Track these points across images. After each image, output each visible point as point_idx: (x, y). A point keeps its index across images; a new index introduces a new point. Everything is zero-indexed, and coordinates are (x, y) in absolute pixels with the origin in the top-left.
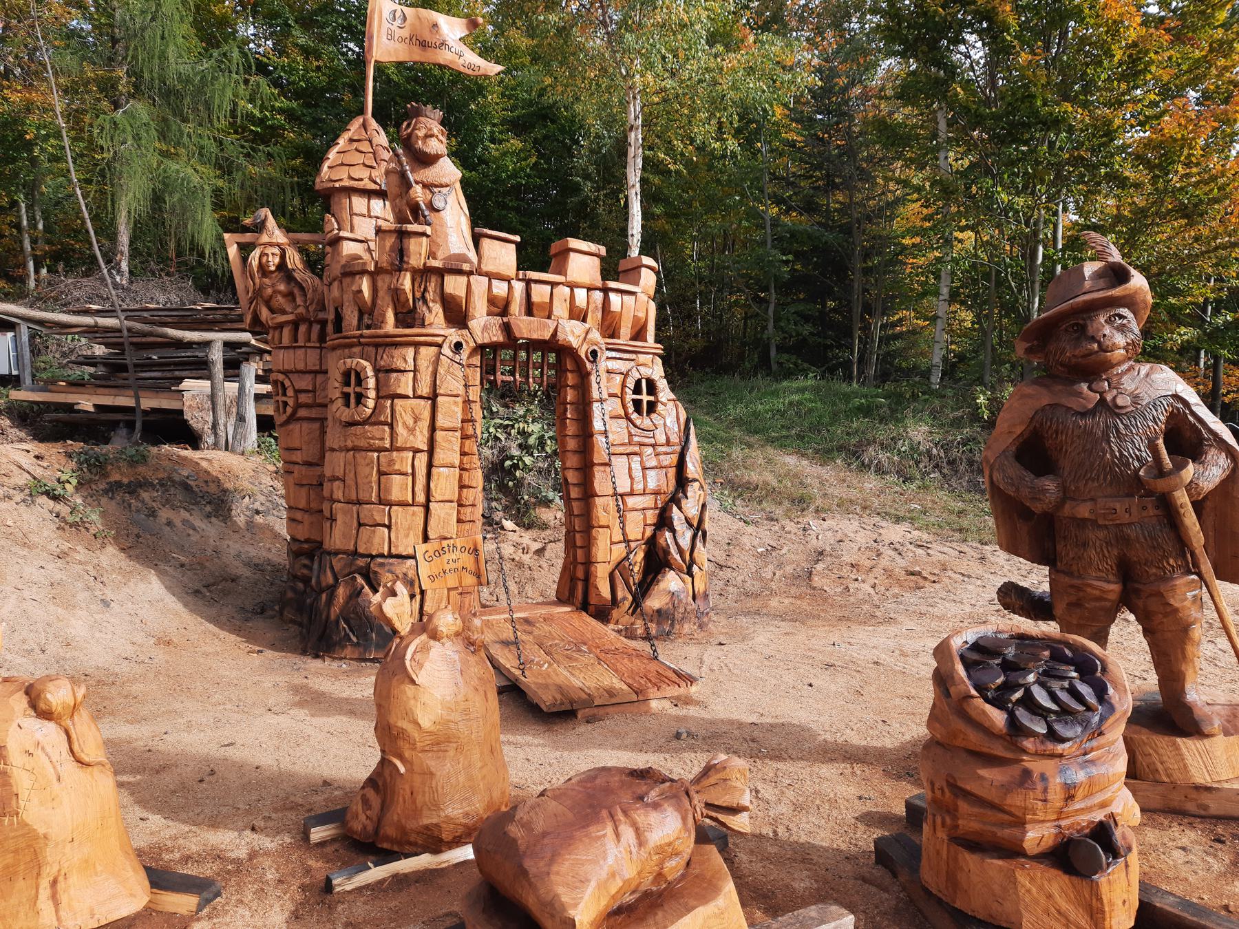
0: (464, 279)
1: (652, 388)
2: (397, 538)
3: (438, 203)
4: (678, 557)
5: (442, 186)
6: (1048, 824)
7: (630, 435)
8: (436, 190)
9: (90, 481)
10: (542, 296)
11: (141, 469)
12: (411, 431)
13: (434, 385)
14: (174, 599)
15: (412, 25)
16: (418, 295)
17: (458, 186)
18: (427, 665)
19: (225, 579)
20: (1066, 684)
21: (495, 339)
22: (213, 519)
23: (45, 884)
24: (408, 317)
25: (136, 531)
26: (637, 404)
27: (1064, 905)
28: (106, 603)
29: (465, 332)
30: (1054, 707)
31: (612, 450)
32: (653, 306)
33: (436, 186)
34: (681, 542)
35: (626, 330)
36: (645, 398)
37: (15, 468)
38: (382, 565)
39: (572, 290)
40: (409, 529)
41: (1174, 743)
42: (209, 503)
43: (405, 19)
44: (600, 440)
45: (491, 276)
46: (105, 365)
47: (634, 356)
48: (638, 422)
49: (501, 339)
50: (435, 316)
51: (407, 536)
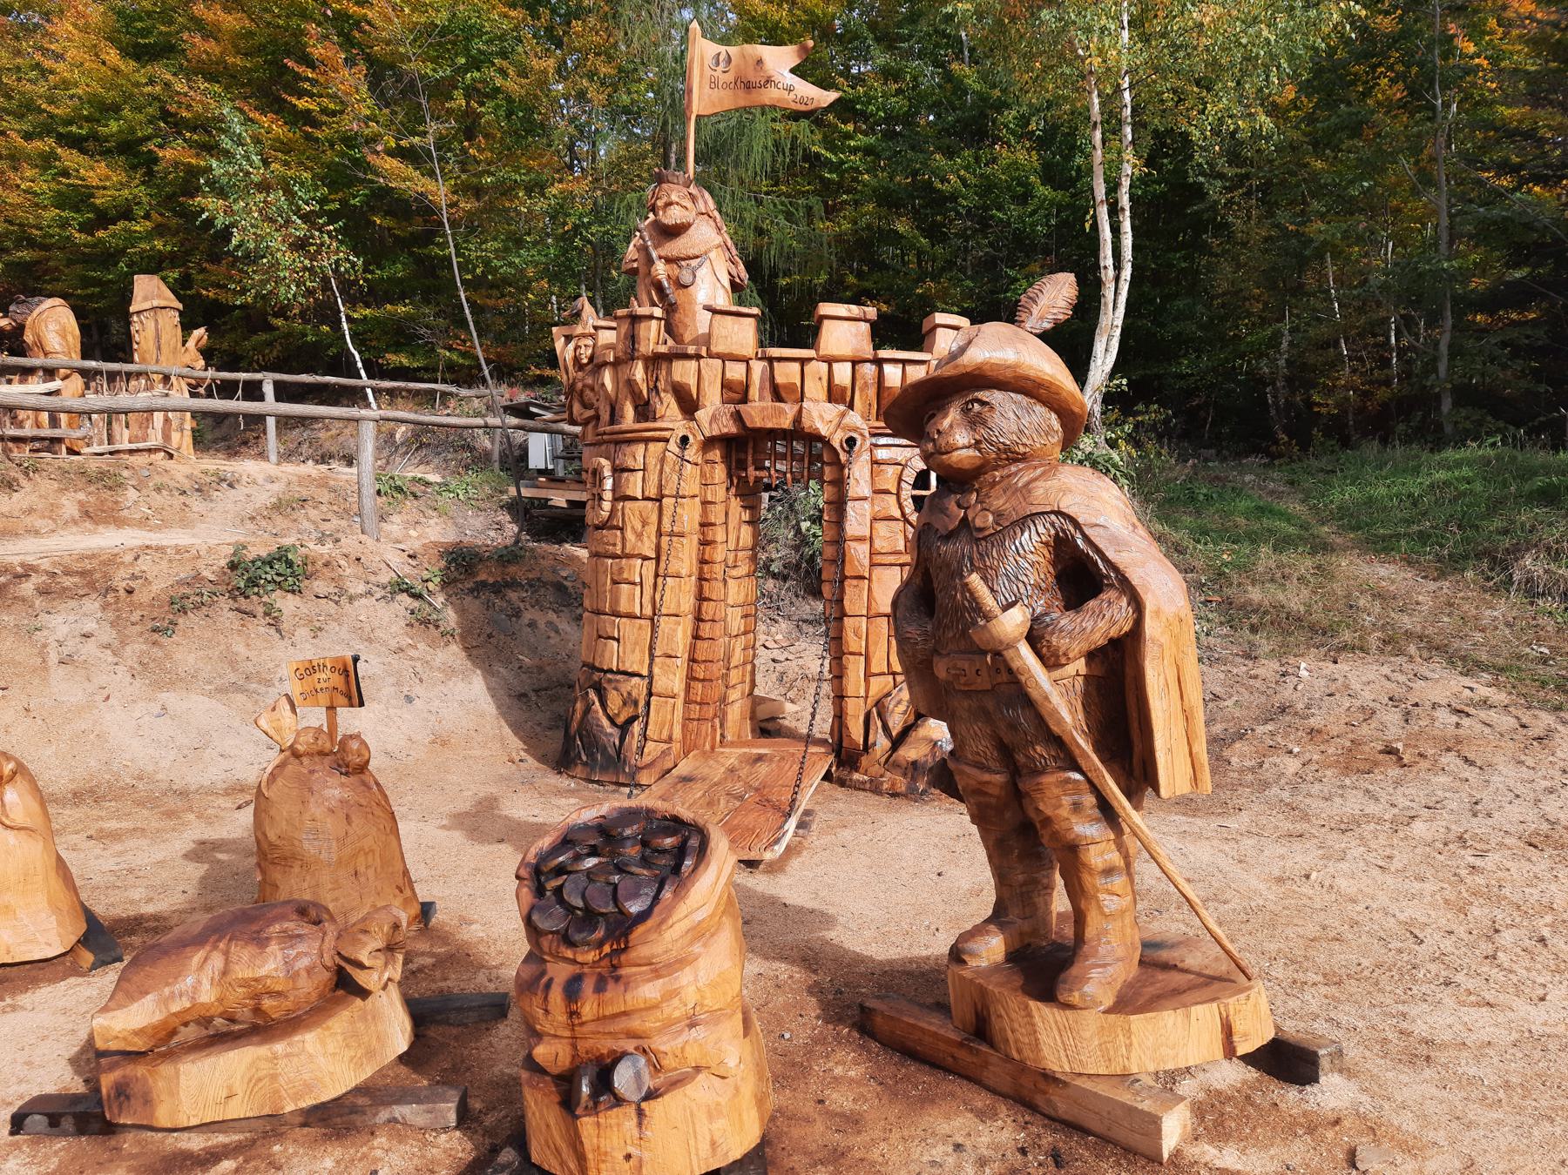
0: (693, 364)
3: (686, 278)
5: (690, 258)
9: (455, 581)
10: (787, 375)
11: (512, 569)
12: (639, 536)
13: (660, 486)
14: (490, 700)
15: (738, 66)
16: (651, 385)
19: (562, 685)
21: (725, 430)
24: (645, 411)
27: (559, 1141)
28: (409, 699)
31: (878, 559)
37: (383, 566)
38: (610, 681)
40: (636, 643)
41: (1027, 1007)
43: (729, 60)
45: (725, 358)
49: (734, 430)
50: (668, 407)
51: (633, 651)
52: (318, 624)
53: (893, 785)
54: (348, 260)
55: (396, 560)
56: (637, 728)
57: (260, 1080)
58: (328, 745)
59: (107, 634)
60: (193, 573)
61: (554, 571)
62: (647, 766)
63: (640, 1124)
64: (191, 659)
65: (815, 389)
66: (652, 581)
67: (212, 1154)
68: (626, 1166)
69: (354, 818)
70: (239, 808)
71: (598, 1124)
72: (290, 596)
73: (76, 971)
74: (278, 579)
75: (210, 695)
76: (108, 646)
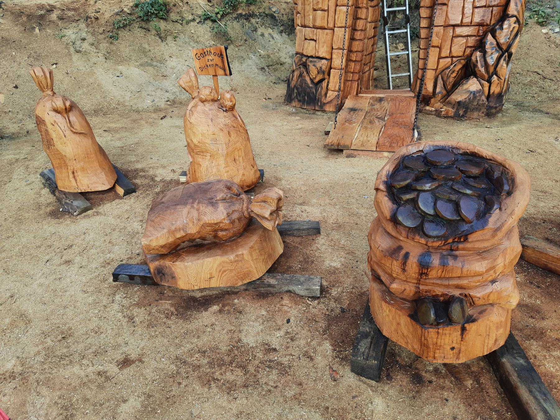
2: (319, 47)
4: (483, 70)
6: (411, 284)
11: (252, 7)
19: (278, 64)
22: (283, 34)
23: (70, 172)
25: (245, 38)
38: (311, 62)
42: (282, 25)
51: (323, 46)
52: (175, 35)
53: (447, 112)
56: (324, 84)
57: (225, 271)
58: (216, 96)
59: (90, 39)
60: (120, 10)
61: (270, 9)
62: (328, 103)
63: (462, 334)
64: (127, 50)
66: (334, 8)
68: (451, 352)
70: (162, 119)
71: (438, 333)
72: (162, 21)
73: (118, 197)
74: (156, 12)
75: (138, 67)
76: (93, 44)
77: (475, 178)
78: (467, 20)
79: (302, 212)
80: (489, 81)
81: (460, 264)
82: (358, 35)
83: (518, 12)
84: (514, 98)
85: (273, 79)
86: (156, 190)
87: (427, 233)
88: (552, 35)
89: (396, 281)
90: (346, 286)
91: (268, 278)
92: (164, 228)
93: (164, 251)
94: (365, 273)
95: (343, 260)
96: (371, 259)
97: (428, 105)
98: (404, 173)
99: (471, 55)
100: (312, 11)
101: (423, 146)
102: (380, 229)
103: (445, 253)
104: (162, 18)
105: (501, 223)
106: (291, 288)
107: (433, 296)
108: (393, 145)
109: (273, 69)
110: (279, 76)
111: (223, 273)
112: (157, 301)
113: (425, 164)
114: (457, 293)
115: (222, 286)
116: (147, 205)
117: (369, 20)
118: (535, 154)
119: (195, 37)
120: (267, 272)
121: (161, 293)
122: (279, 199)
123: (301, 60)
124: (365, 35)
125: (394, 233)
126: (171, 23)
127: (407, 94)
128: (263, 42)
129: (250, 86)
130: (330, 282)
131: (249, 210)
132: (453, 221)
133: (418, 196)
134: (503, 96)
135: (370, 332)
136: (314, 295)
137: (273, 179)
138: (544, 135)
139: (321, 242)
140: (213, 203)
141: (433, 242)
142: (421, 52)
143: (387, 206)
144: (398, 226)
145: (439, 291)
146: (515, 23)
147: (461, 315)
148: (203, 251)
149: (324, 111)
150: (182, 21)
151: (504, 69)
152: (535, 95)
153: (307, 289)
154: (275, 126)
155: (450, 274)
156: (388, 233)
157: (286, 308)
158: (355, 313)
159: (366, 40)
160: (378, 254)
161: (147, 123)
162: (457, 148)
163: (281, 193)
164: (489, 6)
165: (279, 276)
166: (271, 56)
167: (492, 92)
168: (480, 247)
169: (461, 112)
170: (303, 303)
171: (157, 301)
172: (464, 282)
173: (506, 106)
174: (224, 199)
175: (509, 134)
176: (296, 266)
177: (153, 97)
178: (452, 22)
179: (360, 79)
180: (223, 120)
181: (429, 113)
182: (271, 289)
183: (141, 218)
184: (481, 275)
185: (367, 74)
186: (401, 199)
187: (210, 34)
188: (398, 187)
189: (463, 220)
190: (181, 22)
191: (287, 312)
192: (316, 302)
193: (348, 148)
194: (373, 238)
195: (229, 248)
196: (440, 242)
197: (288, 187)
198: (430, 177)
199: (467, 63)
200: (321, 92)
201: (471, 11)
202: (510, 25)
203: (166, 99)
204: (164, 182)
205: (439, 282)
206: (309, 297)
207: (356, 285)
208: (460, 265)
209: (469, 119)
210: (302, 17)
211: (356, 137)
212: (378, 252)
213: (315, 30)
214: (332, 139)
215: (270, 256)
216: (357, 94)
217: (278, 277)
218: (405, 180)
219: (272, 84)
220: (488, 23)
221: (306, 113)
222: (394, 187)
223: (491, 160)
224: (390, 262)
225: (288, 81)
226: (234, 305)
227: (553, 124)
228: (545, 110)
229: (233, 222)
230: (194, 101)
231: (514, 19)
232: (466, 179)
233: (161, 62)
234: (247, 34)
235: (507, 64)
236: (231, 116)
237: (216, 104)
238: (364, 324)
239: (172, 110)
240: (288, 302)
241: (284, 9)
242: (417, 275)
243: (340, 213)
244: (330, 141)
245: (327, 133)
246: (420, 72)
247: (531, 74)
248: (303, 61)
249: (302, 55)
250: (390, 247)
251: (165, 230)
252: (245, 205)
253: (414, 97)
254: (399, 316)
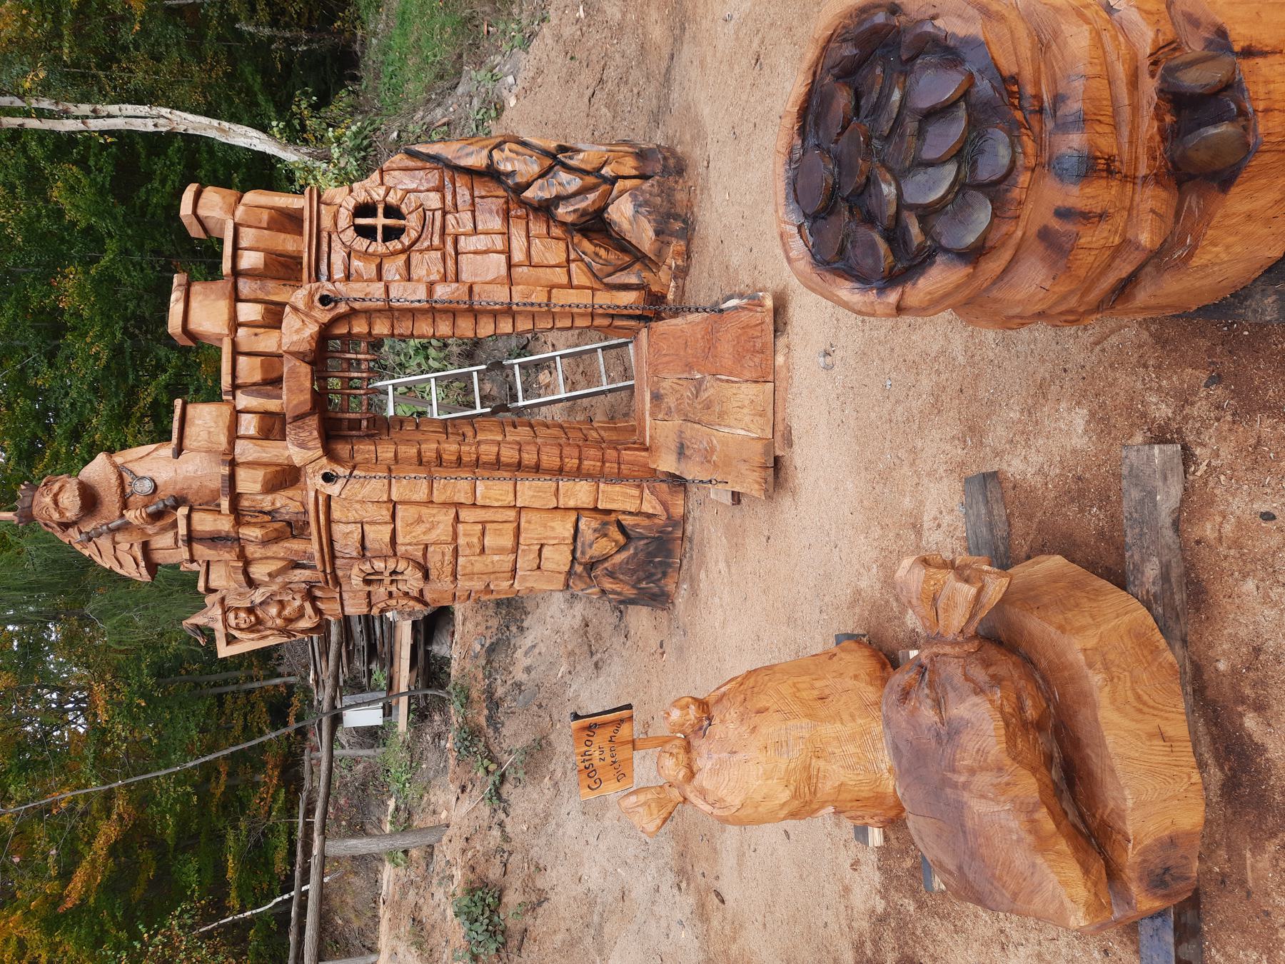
1: (365, 209)
2: (555, 538)
4: (592, 197)
6: (1137, 198)
7: (431, 248)
8: (128, 490)
10: (252, 369)
11: (474, 694)
17: (119, 458)
18: (722, 793)
20: (911, 126)
21: (315, 433)
22: (525, 624)
24: (295, 529)
26: (392, 234)
29: (309, 470)
30: (950, 171)
31: (451, 274)
32: (251, 197)
33: (123, 490)
34: (572, 188)
35: (288, 243)
36: (380, 221)
38: (583, 553)
39: (241, 325)
44: (441, 291)
45: (233, 434)
46: (369, 663)
47: (325, 234)
48: (414, 234)
51: (553, 529)
52: (533, 868)
53: (679, 254)
54: (179, 917)
55: (466, 805)
56: (628, 521)
57: (1139, 698)
58: (677, 742)
62: (667, 510)
63: (1264, 54)
65: (268, 342)
66: (479, 511)
67: (1229, 750)
69: (760, 705)
70: (723, 902)
71: (1267, 111)
72: (505, 900)
77: (858, 96)
78: (499, 242)
79: (939, 526)
80: (613, 181)
81: (1076, 84)
82: (529, 457)
83: (483, 148)
84: (641, 133)
85: (617, 641)
86: (912, 909)
87: (1004, 171)
88: (520, 87)
89: (1129, 235)
90: (1139, 385)
91: (1142, 584)
92: (1034, 865)
93: (1098, 866)
94: (1096, 344)
95: (1063, 405)
96: (1070, 312)
97: (664, 297)
98: (856, 255)
99: (563, 224)
100: (484, 557)
101: (788, 228)
102: (995, 293)
103: (1050, 125)
104: (500, 900)
105: (969, 7)
106: (1165, 519)
107: (1164, 139)
108: (759, 345)
109: (597, 641)
110: (610, 628)
111: (1145, 704)
112: (1249, 894)
113: (830, 214)
114: (1150, 86)
115: (1182, 706)
116: (957, 932)
117: (499, 438)
118: (763, 51)
119: (537, 821)
120: (1124, 588)
121: (1223, 882)
122: (925, 562)
123: (580, 576)
124: (529, 444)
125: (1006, 255)
126: (509, 877)
127: (640, 351)
128: (543, 668)
129: (636, 691)
130: (1132, 425)
131: (960, 639)
132: (969, 115)
133: (912, 207)
134: (642, 150)
135: (1276, 292)
136: (1178, 460)
137: (857, 610)
138: (720, 48)
139: (1017, 466)
140: (950, 733)
141: (1024, 153)
142: (559, 325)
143: (939, 278)
144: (989, 244)
145: (1148, 127)
146: (503, 151)
147: (1210, 64)
148: (1085, 759)
149: (684, 518)
150: (503, 852)
151: (588, 155)
152: (635, 91)
153: (1165, 479)
154: (724, 624)
155: (1105, 103)
156: (1005, 271)
157: (1228, 528)
158: (1218, 349)
159: (539, 441)
160: (1062, 289)
161: (734, 940)
162: (791, 152)
163: (907, 562)
164: (473, 204)
165: (1133, 556)
166: (570, 648)
167: (634, 172)
168: (1029, 45)
169: (677, 225)
170: (1206, 484)
171: (1249, 894)
172: (1121, 71)
173: (659, 139)
174: (938, 705)
175: (720, 116)
176: (1095, 517)
177: (673, 924)
178: (503, 271)
179: (615, 446)
180: (732, 726)
181: (681, 291)
182: (1175, 573)
183: (996, 949)
184: (1097, 36)
185: (605, 439)
186: (921, 248)
187: (530, 788)
188: (891, 259)
189: (965, 95)
190: (506, 855)
191: (1239, 524)
192: (1198, 451)
193: (769, 445)
194: (1017, 310)
195: (1070, 689)
196: (1025, 138)
197: (874, 570)
198: (862, 193)
199: (579, 231)
200: (644, 527)
201: (482, 237)
202: (507, 159)
203: (675, 891)
204: (887, 890)
205: (1125, 131)
206: (1185, 472)
207: (1134, 360)
208: (1079, 85)
209: (690, 206)
210: (497, 579)
211: (743, 432)
212: (1056, 289)
213: (521, 547)
214: (750, 484)
215: (1076, 585)
216: (647, 450)
217: (1136, 557)
218: (873, 246)
219: (629, 643)
220: (503, 200)
221: (691, 557)
222: (891, 269)
223: (815, 73)
224: (1082, 254)
225: (623, 604)
226: (1234, 671)
227: (694, 38)
228: (664, 65)
229: (997, 680)
230: (691, 797)
231: (496, 154)
232: (863, 113)
233: (592, 904)
234: (526, 703)
235: (578, 151)
236: (720, 706)
237: (696, 742)
238: (1255, 311)
239: (700, 877)
240: (1209, 526)
241: (477, 625)
242: (1114, 183)
243: (936, 434)
244: (757, 486)
245: (736, 497)
246: (597, 322)
247: (593, 109)
248: (585, 569)
249: (570, 573)
250: (1043, 259)
251: (1039, 860)
252: (948, 649)
253: (649, 328)
254: (1226, 216)
